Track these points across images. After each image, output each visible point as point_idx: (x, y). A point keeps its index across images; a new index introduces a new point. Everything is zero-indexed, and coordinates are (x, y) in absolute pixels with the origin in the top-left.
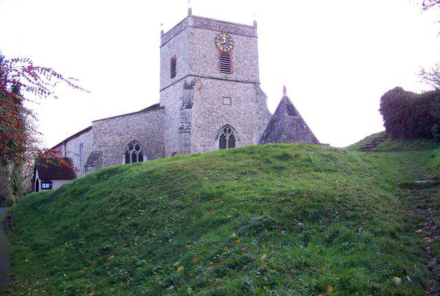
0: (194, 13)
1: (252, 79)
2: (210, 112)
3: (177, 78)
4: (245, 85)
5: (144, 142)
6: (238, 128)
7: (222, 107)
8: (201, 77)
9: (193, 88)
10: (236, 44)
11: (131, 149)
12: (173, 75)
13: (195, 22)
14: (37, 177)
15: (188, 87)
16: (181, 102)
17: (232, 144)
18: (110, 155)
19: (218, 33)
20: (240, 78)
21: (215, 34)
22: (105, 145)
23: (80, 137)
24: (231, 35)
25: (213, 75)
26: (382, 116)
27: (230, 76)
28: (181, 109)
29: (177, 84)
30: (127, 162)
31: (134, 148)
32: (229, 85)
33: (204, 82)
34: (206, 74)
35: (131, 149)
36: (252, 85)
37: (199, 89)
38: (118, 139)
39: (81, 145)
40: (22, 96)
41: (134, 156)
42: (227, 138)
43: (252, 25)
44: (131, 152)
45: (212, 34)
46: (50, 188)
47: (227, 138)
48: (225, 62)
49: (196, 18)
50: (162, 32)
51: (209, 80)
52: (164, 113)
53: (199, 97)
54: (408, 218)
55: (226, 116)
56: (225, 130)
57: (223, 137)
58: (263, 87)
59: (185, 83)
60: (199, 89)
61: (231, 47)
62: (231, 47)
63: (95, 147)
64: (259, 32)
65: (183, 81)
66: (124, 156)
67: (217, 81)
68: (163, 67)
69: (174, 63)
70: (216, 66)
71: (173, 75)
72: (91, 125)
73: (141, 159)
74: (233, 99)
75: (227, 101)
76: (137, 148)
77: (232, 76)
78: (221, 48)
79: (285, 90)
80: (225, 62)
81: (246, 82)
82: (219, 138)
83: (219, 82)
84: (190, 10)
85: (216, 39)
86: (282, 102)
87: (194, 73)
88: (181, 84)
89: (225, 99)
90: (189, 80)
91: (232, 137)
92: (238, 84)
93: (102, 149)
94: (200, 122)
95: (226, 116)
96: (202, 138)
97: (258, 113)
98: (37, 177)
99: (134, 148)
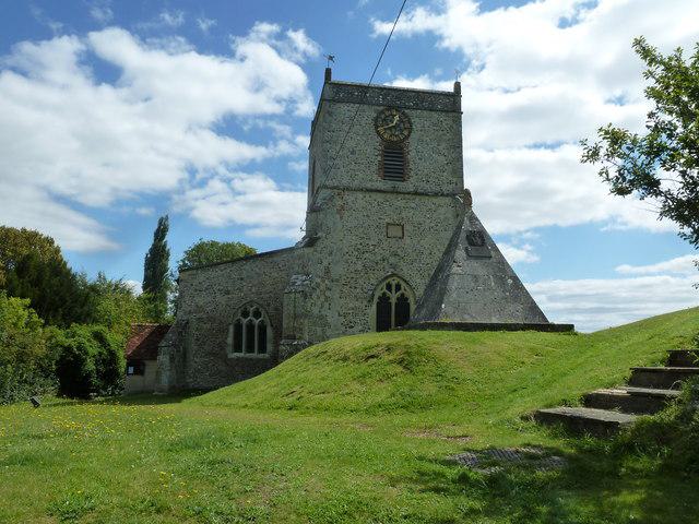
0: (335, 78)
1: (446, 188)
5: (269, 305)
7: (385, 245)
22: (199, 309)
25: (369, 185)
27: (401, 186)
32: (399, 202)
33: (350, 198)
35: (245, 314)
36: (448, 200)
37: (339, 212)
38: (222, 299)
40: (672, 217)
42: (393, 301)
44: (245, 321)
45: (370, 113)
47: (393, 301)
48: (394, 162)
49: (339, 86)
51: (360, 195)
55: (392, 260)
57: (384, 301)
60: (339, 212)
62: (406, 133)
64: (466, 104)
66: (231, 329)
67: (374, 195)
70: (374, 168)
74: (407, 227)
76: (257, 314)
77: (409, 186)
80: (394, 162)
81: (436, 195)
82: (376, 300)
83: (379, 197)
84: (328, 72)
85: (376, 120)
91: (403, 301)
92: (418, 198)
95: (392, 260)
96: (342, 301)
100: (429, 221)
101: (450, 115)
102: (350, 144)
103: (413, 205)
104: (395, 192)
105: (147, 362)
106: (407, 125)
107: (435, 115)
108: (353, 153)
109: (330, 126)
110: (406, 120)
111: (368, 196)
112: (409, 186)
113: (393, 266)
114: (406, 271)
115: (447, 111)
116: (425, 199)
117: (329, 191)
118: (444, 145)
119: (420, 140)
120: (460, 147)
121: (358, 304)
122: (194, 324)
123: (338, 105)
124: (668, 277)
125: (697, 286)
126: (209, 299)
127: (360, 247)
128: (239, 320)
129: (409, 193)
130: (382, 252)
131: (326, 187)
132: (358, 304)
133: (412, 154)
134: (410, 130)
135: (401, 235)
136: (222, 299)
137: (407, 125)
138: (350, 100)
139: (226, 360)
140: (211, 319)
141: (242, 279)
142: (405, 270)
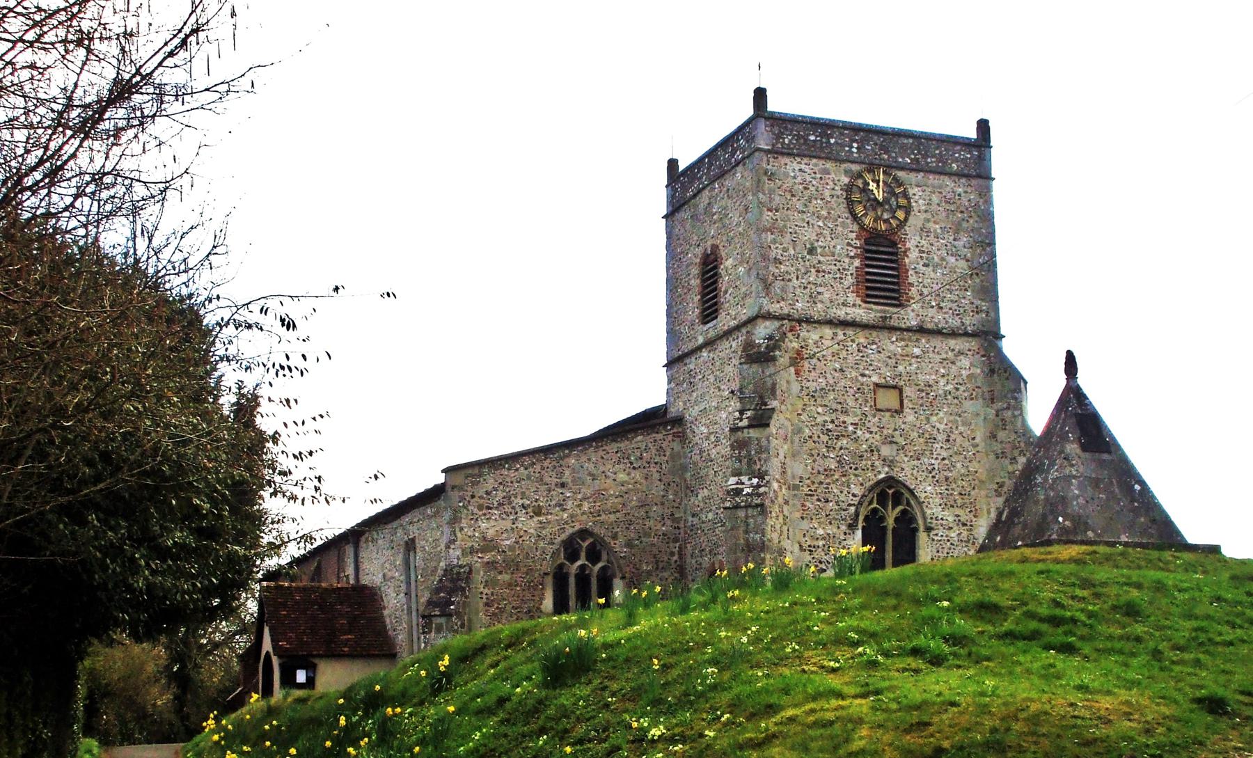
0: (773, 106)
2: (834, 433)
3: (725, 321)
4: (952, 342)
5: (615, 537)
6: (926, 490)
8: (800, 321)
9: (774, 359)
10: (919, 202)
11: (573, 556)
12: (710, 311)
13: (779, 137)
14: (267, 646)
15: (759, 357)
16: (735, 404)
17: (907, 553)
18: (505, 577)
19: (855, 168)
20: (936, 318)
21: (846, 172)
22: (488, 545)
23: (406, 519)
24: (900, 174)
25: (841, 313)
26: (405, 499)
28: (734, 429)
29: (725, 344)
30: (561, 606)
31: (583, 554)
32: (892, 344)
33: (812, 335)
34: (818, 311)
35: (573, 556)
36: (973, 344)
39: (410, 546)
41: (583, 578)
42: (890, 522)
43: (972, 133)
44: (574, 568)
46: (310, 683)
47: (890, 522)
49: (783, 122)
50: (672, 164)
51: (828, 331)
52: (682, 437)
53: (795, 387)
54: (693, 528)
55: (886, 451)
56: (882, 498)
58: (1011, 348)
59: (749, 345)
61: (901, 215)
62: (901, 215)
63: (455, 553)
65: (742, 337)
66: (549, 581)
68: (674, 284)
69: (710, 266)
70: (849, 280)
71: (710, 311)
72: (440, 479)
73: (606, 590)
74: (908, 391)
75: (888, 399)
77: (910, 316)
78: (868, 221)
79: (1071, 363)
84: (760, 95)
86: (1062, 403)
87: (775, 308)
88: (734, 345)
89: (881, 392)
90: (763, 330)
93: (477, 561)
94: (798, 469)
95: (886, 451)
96: (805, 525)
97: (993, 436)
98: (267, 646)
99: (583, 554)
100: (942, 382)
101: (974, 182)
102: (808, 235)
103: (917, 351)
104: (883, 326)
105: (316, 661)
106: (902, 202)
107: (948, 182)
108: (812, 251)
109: (771, 200)
110: (895, 189)
111: (840, 333)
112: (910, 316)
113: (886, 461)
114: (907, 473)
115: (968, 176)
116: (937, 342)
117: (777, 324)
118: (965, 239)
119: (923, 230)
120: (992, 244)
121: (831, 530)
122: (479, 577)
123: (787, 160)
124: (849, 164)
125: (1249, 594)
126: (507, 524)
127: (831, 426)
128: (561, 566)
129: (908, 330)
130: (868, 435)
131: (768, 316)
132: (831, 530)
133: (913, 254)
134: (908, 210)
135: (897, 406)
136: (529, 525)
137: (898, 197)
138: (806, 151)
139: (843, 593)
140: (512, 565)
141: (563, 485)
142: (908, 471)
